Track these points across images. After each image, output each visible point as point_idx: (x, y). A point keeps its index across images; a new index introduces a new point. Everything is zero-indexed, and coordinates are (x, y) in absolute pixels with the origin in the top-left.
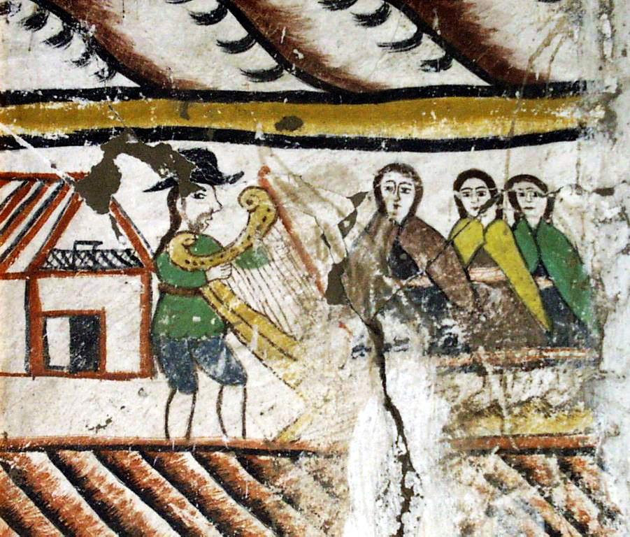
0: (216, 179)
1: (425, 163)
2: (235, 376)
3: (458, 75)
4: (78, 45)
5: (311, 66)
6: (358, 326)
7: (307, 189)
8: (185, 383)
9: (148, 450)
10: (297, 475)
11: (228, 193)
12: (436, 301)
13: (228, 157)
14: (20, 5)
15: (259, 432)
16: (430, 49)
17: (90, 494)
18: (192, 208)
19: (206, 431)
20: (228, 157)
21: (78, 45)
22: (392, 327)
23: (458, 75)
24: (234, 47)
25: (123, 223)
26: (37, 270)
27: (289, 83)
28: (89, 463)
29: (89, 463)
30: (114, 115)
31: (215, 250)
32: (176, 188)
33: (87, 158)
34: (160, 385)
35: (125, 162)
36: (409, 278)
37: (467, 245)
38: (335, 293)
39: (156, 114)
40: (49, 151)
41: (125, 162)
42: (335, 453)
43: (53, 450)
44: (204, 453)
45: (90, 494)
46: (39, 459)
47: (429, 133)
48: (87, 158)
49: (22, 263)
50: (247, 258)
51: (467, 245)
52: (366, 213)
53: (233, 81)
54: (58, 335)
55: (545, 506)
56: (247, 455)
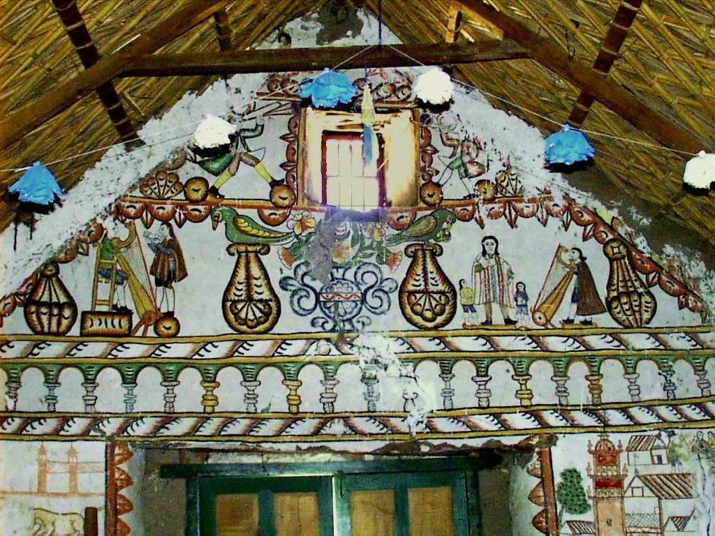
0: (674, 434)
1: (703, 431)
2: (680, 464)
3: (707, 417)
4: (654, 416)
5: (686, 417)
6: (696, 455)
7: (687, 436)
8: (674, 465)
9: (670, 475)
10: (690, 477)
11: (677, 437)
12: (707, 451)
13: (676, 431)
14: (458, 115)
15: (684, 472)
16: (703, 414)
17: (663, 482)
18: (672, 439)
19: (677, 472)
20: (676, 431)
21: (654, 416)
22: (701, 456)
23: (707, 417)
24: (689, 341)
25: (662, 441)
26: (651, 449)
27: (683, 419)
28: (662, 477)
29: (662, 477)
30: (660, 426)
31: (676, 445)
32: (669, 436)
33: (657, 432)
34: (670, 465)
35: (663, 433)
36: (458, 444)
37: (710, 443)
38: (693, 451)
39: (666, 425)
40: (310, 127)
41: (663, 433)
42: (695, 474)
43: (657, 475)
44: (677, 475)
45: (663, 482)
46: (655, 477)
47: (704, 426)
48: (657, 432)
49: (649, 448)
50: (680, 446)
51: (710, 443)
52: (696, 439)
53: (675, 420)
54: (656, 459)
55: (593, 405)
56: (683, 475)
